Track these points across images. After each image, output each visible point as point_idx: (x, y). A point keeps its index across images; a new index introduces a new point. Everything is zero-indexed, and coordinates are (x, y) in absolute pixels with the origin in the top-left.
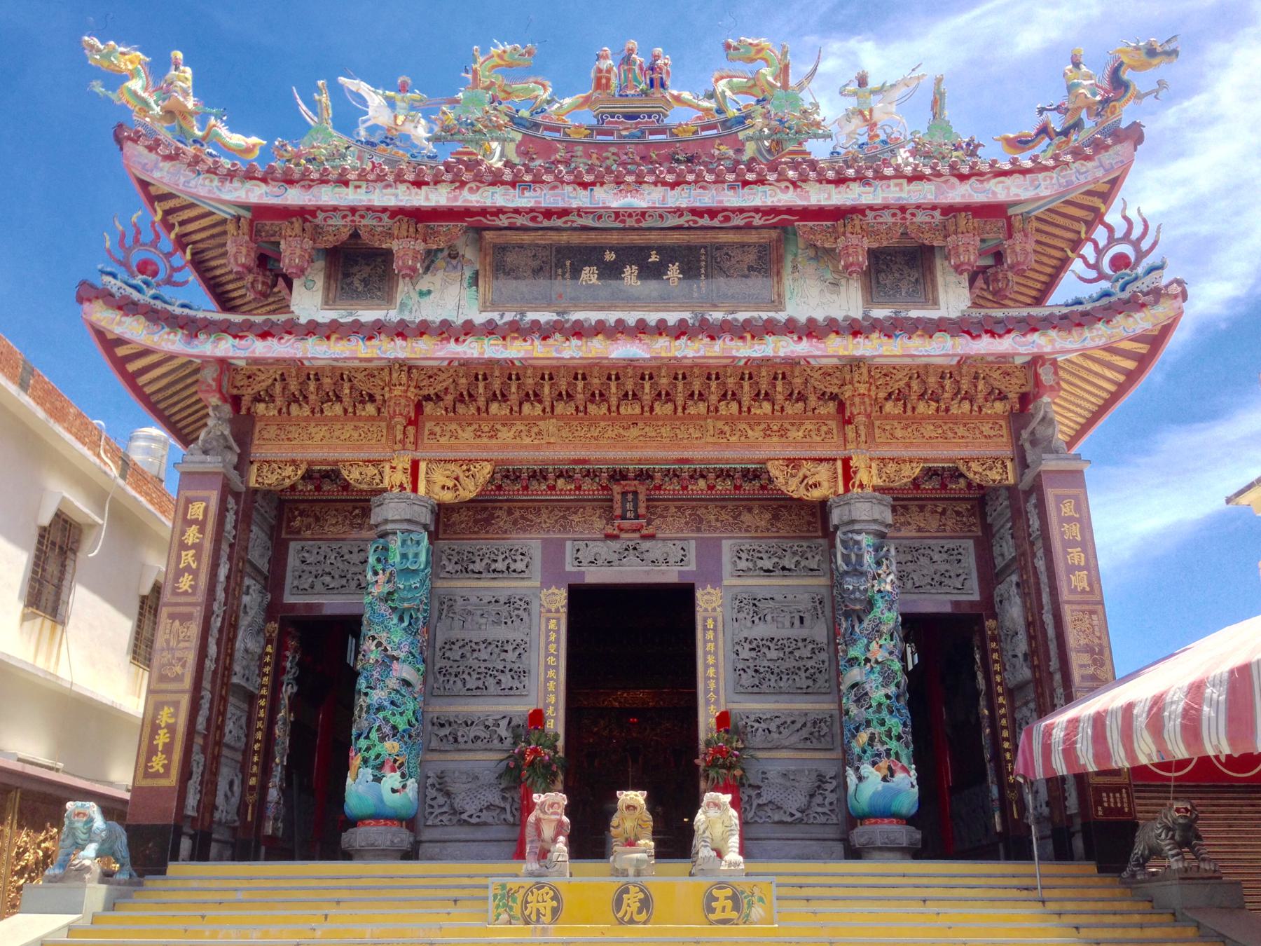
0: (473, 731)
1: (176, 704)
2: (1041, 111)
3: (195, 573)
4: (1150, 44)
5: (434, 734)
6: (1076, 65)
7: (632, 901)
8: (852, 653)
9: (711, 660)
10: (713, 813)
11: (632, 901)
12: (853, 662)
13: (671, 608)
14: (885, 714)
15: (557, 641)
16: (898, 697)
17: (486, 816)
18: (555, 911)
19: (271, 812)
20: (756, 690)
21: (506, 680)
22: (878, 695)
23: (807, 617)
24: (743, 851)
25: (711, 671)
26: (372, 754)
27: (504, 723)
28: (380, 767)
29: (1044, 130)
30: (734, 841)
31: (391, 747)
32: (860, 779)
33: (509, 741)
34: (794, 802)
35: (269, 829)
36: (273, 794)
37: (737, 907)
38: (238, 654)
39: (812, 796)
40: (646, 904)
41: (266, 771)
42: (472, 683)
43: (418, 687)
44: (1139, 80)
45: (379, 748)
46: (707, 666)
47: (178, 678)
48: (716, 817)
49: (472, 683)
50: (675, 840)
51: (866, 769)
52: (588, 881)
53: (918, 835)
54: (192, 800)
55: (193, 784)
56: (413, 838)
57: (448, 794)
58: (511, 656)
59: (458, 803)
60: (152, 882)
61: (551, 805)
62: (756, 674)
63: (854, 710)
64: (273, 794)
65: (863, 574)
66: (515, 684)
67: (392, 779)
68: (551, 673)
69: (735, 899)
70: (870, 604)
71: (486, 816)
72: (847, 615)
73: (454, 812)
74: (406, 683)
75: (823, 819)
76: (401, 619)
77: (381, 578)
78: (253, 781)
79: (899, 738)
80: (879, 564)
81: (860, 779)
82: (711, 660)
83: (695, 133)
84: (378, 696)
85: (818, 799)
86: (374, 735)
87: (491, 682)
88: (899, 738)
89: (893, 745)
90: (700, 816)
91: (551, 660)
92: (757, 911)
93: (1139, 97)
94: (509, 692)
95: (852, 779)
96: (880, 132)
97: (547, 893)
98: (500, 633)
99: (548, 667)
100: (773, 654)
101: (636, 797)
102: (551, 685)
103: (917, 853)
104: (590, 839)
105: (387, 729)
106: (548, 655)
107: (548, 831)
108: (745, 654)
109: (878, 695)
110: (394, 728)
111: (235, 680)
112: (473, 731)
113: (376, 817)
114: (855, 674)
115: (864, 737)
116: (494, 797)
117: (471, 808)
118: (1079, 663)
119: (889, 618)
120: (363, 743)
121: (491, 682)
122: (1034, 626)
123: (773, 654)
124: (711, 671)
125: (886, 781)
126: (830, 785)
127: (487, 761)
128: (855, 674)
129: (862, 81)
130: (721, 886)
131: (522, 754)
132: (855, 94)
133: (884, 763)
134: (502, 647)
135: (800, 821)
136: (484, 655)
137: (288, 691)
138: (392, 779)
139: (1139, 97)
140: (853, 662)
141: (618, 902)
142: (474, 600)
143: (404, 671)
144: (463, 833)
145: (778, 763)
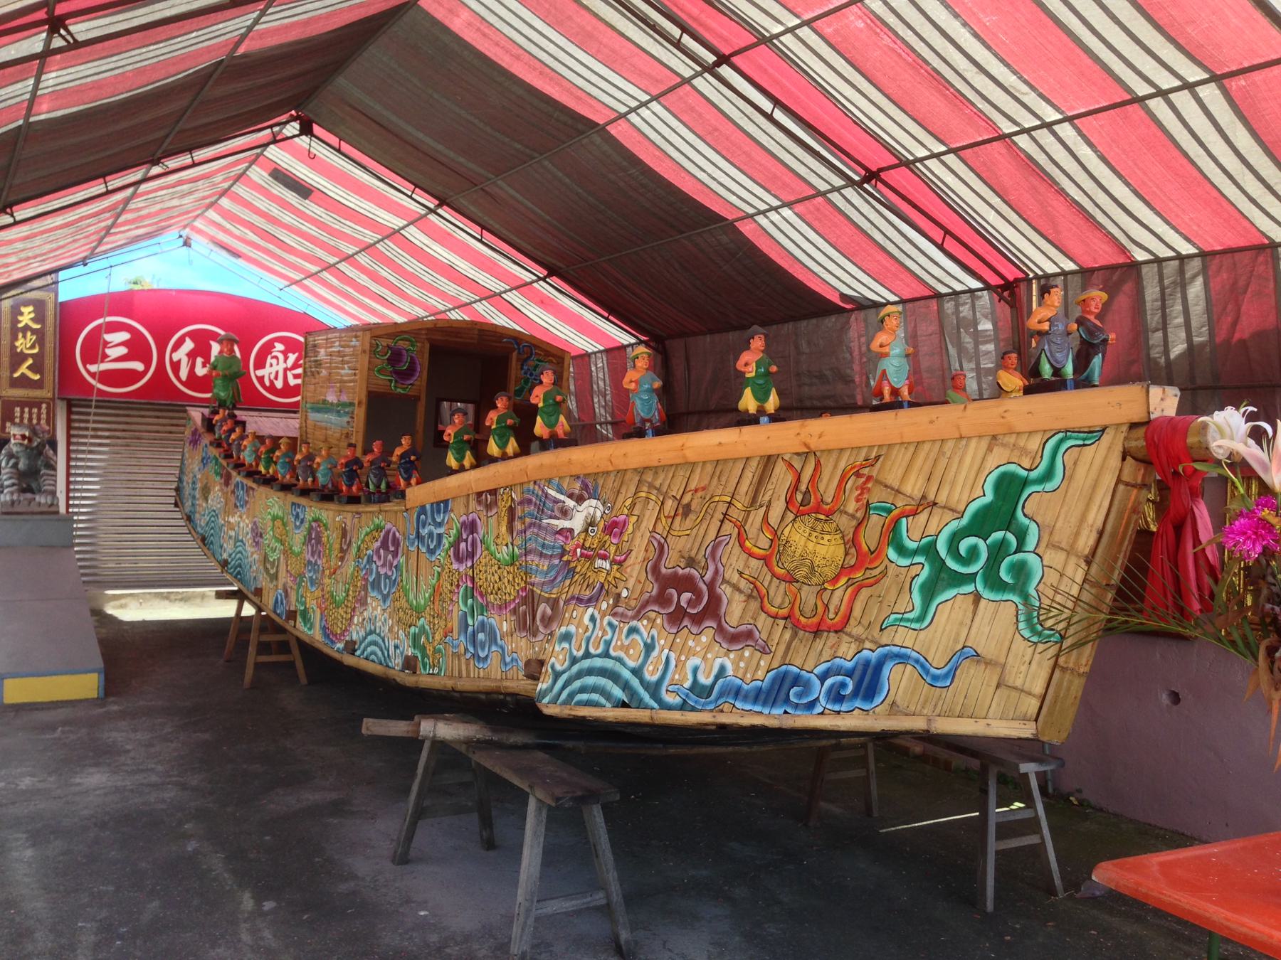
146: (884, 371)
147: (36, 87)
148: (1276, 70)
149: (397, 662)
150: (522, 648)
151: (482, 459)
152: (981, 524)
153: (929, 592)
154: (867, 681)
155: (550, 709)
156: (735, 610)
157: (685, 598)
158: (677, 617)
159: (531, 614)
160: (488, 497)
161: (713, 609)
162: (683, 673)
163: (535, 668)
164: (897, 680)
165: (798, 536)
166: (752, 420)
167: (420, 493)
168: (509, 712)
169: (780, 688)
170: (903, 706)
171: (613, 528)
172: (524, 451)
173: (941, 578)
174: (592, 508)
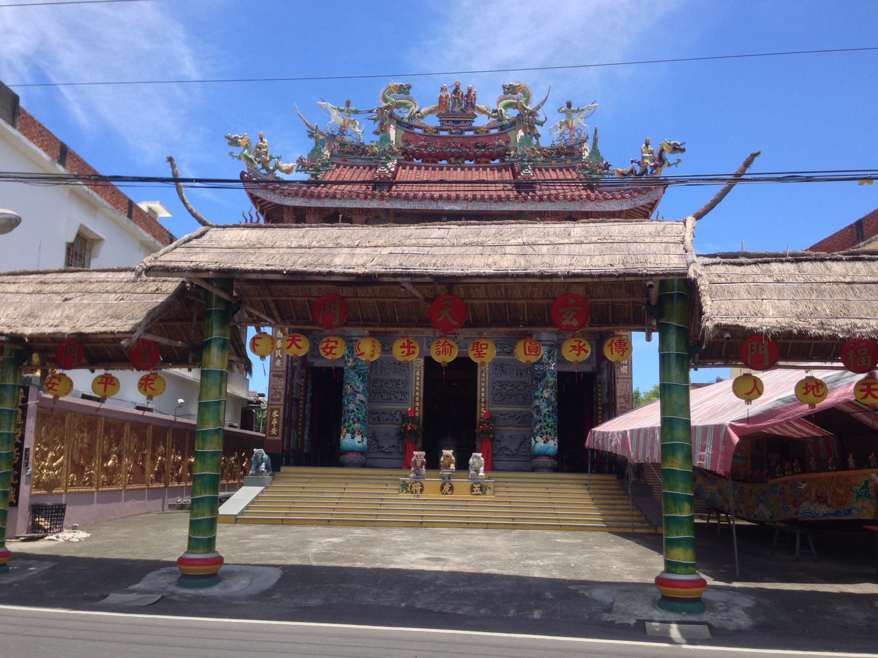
0: (386, 416)
1: (279, 410)
2: (632, 162)
3: (282, 359)
4: (676, 144)
5: (373, 417)
6: (647, 145)
7: (447, 487)
8: (536, 394)
9: (483, 390)
10: (475, 460)
11: (447, 487)
12: (537, 397)
13: (465, 368)
14: (547, 418)
15: (420, 380)
16: (552, 411)
17: (392, 450)
18: (421, 490)
19: (306, 443)
20: (501, 403)
21: (399, 396)
22: (545, 411)
23: (524, 373)
24: (485, 470)
25: (483, 394)
26: (350, 429)
27: (398, 414)
28: (353, 433)
29: (632, 172)
30: (482, 468)
31: (357, 426)
32: (536, 442)
33: (400, 421)
34: (513, 447)
35: (305, 451)
36: (306, 437)
37: (481, 490)
38: (295, 385)
39: (521, 445)
40: (451, 489)
41: (304, 427)
42: (385, 397)
43: (367, 402)
44: (669, 157)
45: (353, 426)
46: (481, 392)
47: (279, 400)
48: (477, 459)
49: (385, 397)
50: (463, 465)
51: (538, 438)
52: (432, 481)
53: (556, 463)
54: (285, 444)
55: (285, 439)
56: (366, 460)
57: (377, 441)
58: (401, 386)
59: (381, 444)
60: (277, 474)
61: (419, 455)
62: (500, 395)
63: (535, 416)
64: (306, 437)
65: (542, 364)
66: (403, 397)
67: (358, 438)
68: (417, 394)
69: (481, 488)
70: (545, 375)
71: (392, 450)
72: (536, 378)
73: (379, 447)
74: (362, 402)
75: (524, 454)
76: (359, 377)
77: (351, 360)
78: (300, 433)
79: (551, 427)
80: (549, 358)
81: (536, 442)
82: (483, 390)
83: (487, 132)
84: (351, 407)
85: (523, 446)
86: (351, 421)
87: (393, 397)
88: (551, 427)
89: (549, 430)
90: (471, 460)
91: (417, 388)
92: (488, 491)
93: (669, 165)
94: (401, 401)
95: (533, 442)
96: (575, 133)
97: (418, 484)
98: (397, 377)
99: (416, 391)
100: (508, 388)
101: (450, 452)
102: (417, 399)
103: (556, 470)
104: (433, 463)
105: (356, 419)
106: (416, 386)
107: (419, 464)
108: (497, 387)
109: (545, 411)
110: (358, 419)
111: (294, 396)
112: (386, 416)
113: (352, 451)
114: (537, 402)
115: (538, 427)
116: (395, 442)
117: (386, 446)
118: (620, 402)
119: (551, 380)
120: (347, 424)
121: (393, 397)
122: (609, 383)
123: (508, 388)
124: (483, 394)
125: (546, 444)
126: (526, 441)
127: (392, 428)
128: (537, 402)
129: (569, 105)
130: (476, 483)
131: (406, 427)
132: (565, 112)
133: (544, 437)
134: (397, 382)
135: (515, 454)
136: (390, 385)
137: (309, 395)
138: (358, 438)
139: (669, 165)
140: (537, 397)
141: (442, 488)
142: (385, 362)
143: (360, 397)
144: (382, 455)
145: (508, 432)
146: (642, 206)
147: (457, 327)
148: (2, 272)
149: (768, 517)
150: (794, 510)
151: (784, 475)
152: (863, 487)
153: (857, 498)
154: (849, 512)
155: (800, 519)
156: (829, 502)
157: (821, 500)
158: (820, 503)
159: (796, 504)
160: (786, 483)
161: (826, 501)
162: (822, 511)
163: (797, 513)
164: (854, 511)
165: (838, 489)
166: (830, 471)
167: (771, 482)
168: (794, 522)
169: (836, 514)
170: (855, 515)
171: (809, 488)
172: (792, 474)
173: (859, 496)
174: (805, 485)
